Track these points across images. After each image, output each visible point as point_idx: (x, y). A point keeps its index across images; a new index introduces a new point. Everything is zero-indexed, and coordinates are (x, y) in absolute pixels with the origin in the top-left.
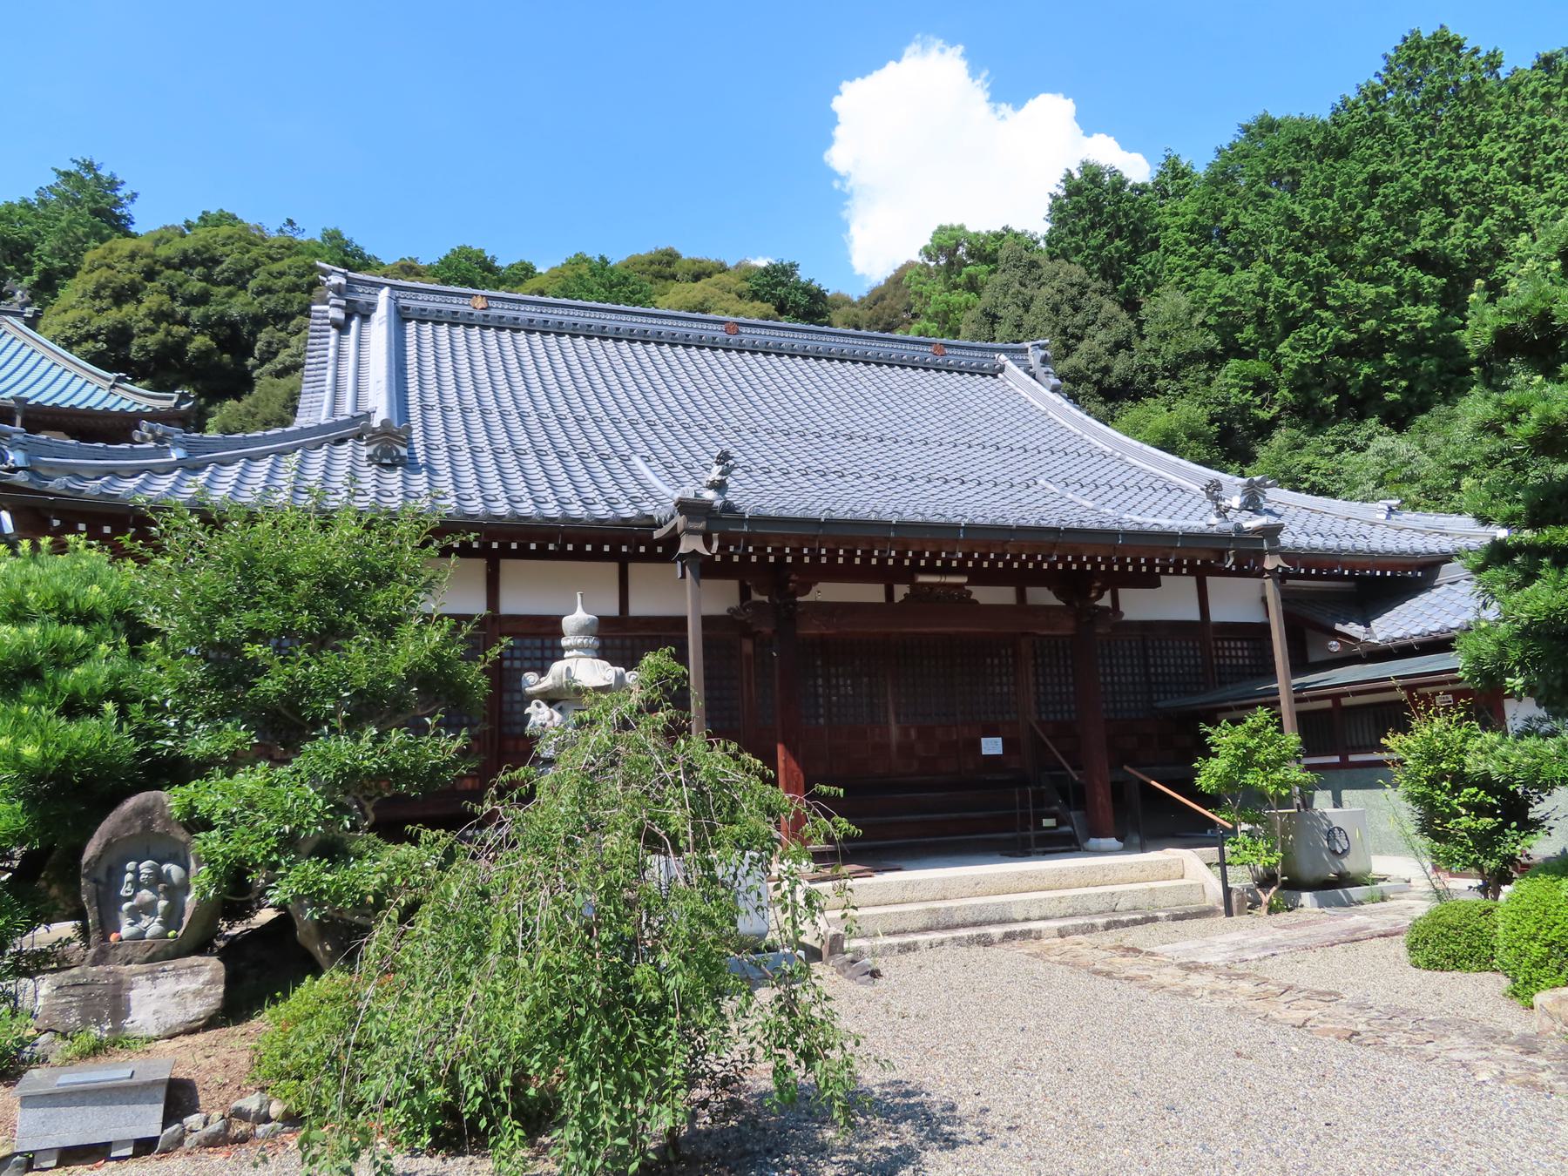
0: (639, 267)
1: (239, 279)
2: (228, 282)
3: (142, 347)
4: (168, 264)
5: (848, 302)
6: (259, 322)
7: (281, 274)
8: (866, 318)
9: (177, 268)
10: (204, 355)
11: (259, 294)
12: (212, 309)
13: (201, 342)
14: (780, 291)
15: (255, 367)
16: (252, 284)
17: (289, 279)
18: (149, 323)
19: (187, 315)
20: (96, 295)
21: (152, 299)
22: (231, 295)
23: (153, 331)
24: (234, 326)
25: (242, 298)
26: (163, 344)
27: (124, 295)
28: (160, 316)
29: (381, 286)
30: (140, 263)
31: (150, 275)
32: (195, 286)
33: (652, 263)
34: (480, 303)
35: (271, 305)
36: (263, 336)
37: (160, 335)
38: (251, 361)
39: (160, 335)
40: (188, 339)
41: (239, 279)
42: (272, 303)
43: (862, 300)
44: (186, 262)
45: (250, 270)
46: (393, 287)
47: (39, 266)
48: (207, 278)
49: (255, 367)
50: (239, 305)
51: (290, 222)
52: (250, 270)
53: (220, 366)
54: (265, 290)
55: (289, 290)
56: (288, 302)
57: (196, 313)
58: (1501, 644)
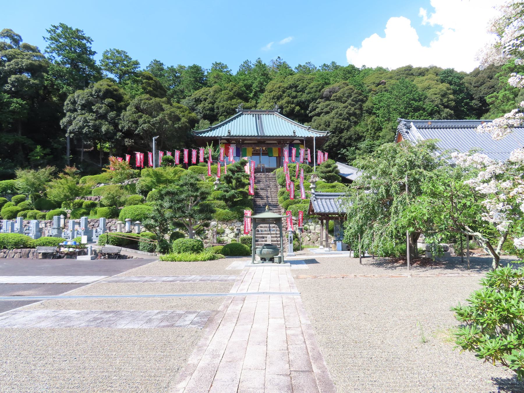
0: (401, 72)
1: (303, 90)
2: (300, 91)
3: (286, 111)
4: (287, 89)
5: (466, 75)
6: (309, 101)
7: (312, 88)
8: (474, 80)
9: (289, 89)
10: (298, 111)
11: (308, 94)
12: (298, 99)
13: (298, 108)
14: (450, 78)
15: (309, 113)
16: (306, 91)
17: (314, 89)
18: (287, 105)
19: (293, 101)
20: (273, 98)
21: (286, 99)
22: (301, 95)
23: (288, 107)
24: (303, 103)
25: (304, 95)
26: (290, 109)
27: (279, 98)
28: (288, 102)
29: (411, 122)
30: (282, 89)
31: (284, 92)
32: (294, 94)
33: (405, 70)
34: (430, 123)
35: (311, 96)
36: (311, 105)
37: (289, 107)
38: (308, 112)
39: (289, 107)
40: (294, 108)
41: (303, 90)
42: (312, 96)
43: (471, 73)
44: (291, 87)
45: (305, 88)
46: (413, 122)
47: (254, 90)
48: (296, 91)
49: (309, 113)
50: (304, 97)
51: (279, 57)
52: (305, 88)
53: (302, 114)
54: (309, 93)
55: (315, 92)
56: (315, 95)
57: (295, 100)
58: (344, 228)
